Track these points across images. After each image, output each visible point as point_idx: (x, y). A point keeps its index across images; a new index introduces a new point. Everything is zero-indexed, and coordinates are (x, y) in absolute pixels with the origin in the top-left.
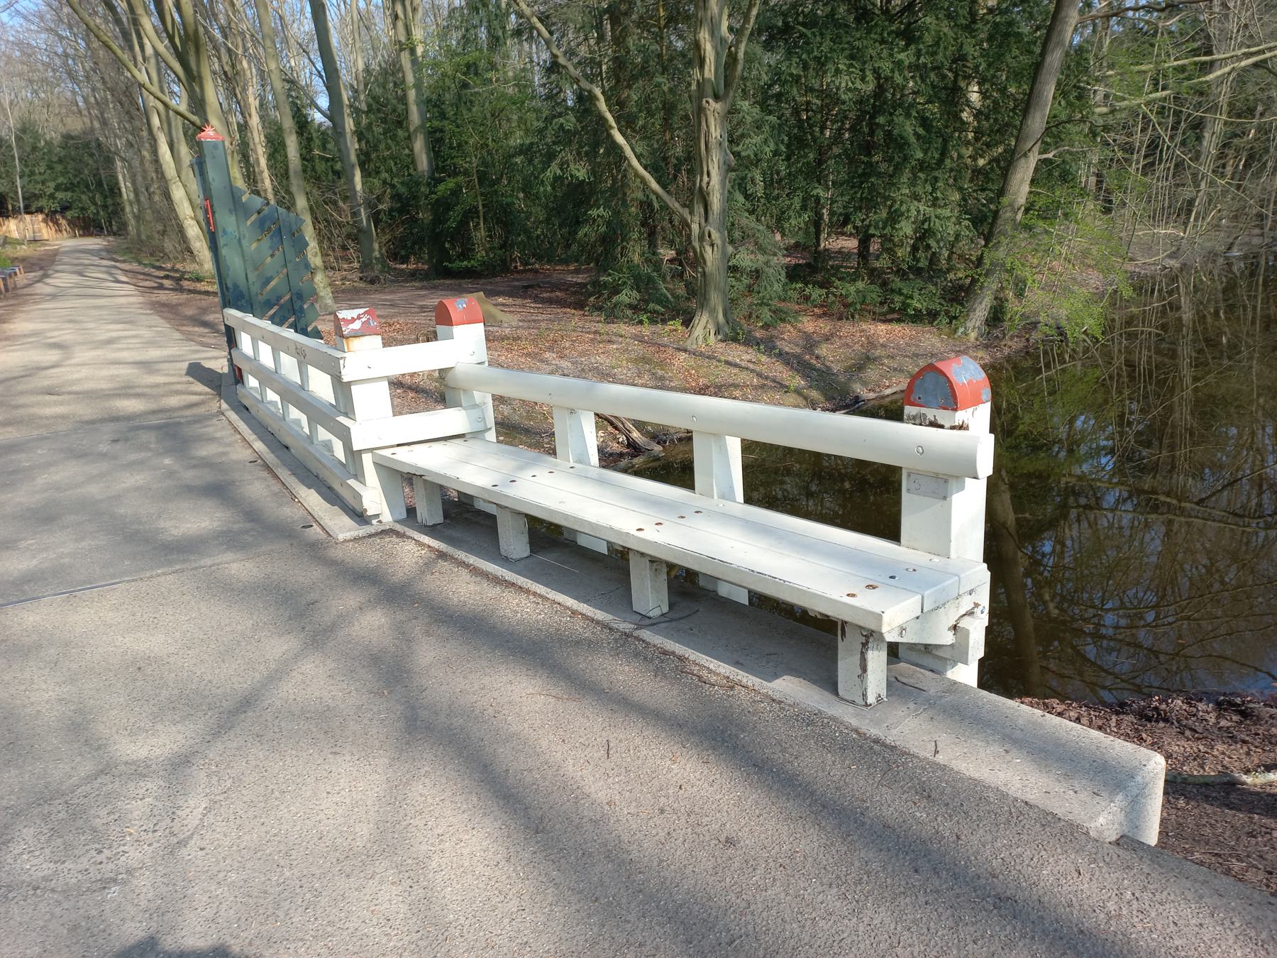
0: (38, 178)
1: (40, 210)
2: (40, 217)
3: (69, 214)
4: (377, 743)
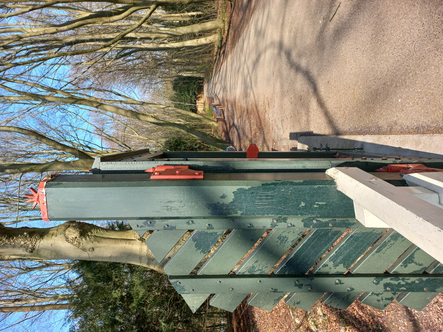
0: (186, 99)
1: (195, 101)
2: (197, 101)
3: (196, 93)
4: (103, 319)
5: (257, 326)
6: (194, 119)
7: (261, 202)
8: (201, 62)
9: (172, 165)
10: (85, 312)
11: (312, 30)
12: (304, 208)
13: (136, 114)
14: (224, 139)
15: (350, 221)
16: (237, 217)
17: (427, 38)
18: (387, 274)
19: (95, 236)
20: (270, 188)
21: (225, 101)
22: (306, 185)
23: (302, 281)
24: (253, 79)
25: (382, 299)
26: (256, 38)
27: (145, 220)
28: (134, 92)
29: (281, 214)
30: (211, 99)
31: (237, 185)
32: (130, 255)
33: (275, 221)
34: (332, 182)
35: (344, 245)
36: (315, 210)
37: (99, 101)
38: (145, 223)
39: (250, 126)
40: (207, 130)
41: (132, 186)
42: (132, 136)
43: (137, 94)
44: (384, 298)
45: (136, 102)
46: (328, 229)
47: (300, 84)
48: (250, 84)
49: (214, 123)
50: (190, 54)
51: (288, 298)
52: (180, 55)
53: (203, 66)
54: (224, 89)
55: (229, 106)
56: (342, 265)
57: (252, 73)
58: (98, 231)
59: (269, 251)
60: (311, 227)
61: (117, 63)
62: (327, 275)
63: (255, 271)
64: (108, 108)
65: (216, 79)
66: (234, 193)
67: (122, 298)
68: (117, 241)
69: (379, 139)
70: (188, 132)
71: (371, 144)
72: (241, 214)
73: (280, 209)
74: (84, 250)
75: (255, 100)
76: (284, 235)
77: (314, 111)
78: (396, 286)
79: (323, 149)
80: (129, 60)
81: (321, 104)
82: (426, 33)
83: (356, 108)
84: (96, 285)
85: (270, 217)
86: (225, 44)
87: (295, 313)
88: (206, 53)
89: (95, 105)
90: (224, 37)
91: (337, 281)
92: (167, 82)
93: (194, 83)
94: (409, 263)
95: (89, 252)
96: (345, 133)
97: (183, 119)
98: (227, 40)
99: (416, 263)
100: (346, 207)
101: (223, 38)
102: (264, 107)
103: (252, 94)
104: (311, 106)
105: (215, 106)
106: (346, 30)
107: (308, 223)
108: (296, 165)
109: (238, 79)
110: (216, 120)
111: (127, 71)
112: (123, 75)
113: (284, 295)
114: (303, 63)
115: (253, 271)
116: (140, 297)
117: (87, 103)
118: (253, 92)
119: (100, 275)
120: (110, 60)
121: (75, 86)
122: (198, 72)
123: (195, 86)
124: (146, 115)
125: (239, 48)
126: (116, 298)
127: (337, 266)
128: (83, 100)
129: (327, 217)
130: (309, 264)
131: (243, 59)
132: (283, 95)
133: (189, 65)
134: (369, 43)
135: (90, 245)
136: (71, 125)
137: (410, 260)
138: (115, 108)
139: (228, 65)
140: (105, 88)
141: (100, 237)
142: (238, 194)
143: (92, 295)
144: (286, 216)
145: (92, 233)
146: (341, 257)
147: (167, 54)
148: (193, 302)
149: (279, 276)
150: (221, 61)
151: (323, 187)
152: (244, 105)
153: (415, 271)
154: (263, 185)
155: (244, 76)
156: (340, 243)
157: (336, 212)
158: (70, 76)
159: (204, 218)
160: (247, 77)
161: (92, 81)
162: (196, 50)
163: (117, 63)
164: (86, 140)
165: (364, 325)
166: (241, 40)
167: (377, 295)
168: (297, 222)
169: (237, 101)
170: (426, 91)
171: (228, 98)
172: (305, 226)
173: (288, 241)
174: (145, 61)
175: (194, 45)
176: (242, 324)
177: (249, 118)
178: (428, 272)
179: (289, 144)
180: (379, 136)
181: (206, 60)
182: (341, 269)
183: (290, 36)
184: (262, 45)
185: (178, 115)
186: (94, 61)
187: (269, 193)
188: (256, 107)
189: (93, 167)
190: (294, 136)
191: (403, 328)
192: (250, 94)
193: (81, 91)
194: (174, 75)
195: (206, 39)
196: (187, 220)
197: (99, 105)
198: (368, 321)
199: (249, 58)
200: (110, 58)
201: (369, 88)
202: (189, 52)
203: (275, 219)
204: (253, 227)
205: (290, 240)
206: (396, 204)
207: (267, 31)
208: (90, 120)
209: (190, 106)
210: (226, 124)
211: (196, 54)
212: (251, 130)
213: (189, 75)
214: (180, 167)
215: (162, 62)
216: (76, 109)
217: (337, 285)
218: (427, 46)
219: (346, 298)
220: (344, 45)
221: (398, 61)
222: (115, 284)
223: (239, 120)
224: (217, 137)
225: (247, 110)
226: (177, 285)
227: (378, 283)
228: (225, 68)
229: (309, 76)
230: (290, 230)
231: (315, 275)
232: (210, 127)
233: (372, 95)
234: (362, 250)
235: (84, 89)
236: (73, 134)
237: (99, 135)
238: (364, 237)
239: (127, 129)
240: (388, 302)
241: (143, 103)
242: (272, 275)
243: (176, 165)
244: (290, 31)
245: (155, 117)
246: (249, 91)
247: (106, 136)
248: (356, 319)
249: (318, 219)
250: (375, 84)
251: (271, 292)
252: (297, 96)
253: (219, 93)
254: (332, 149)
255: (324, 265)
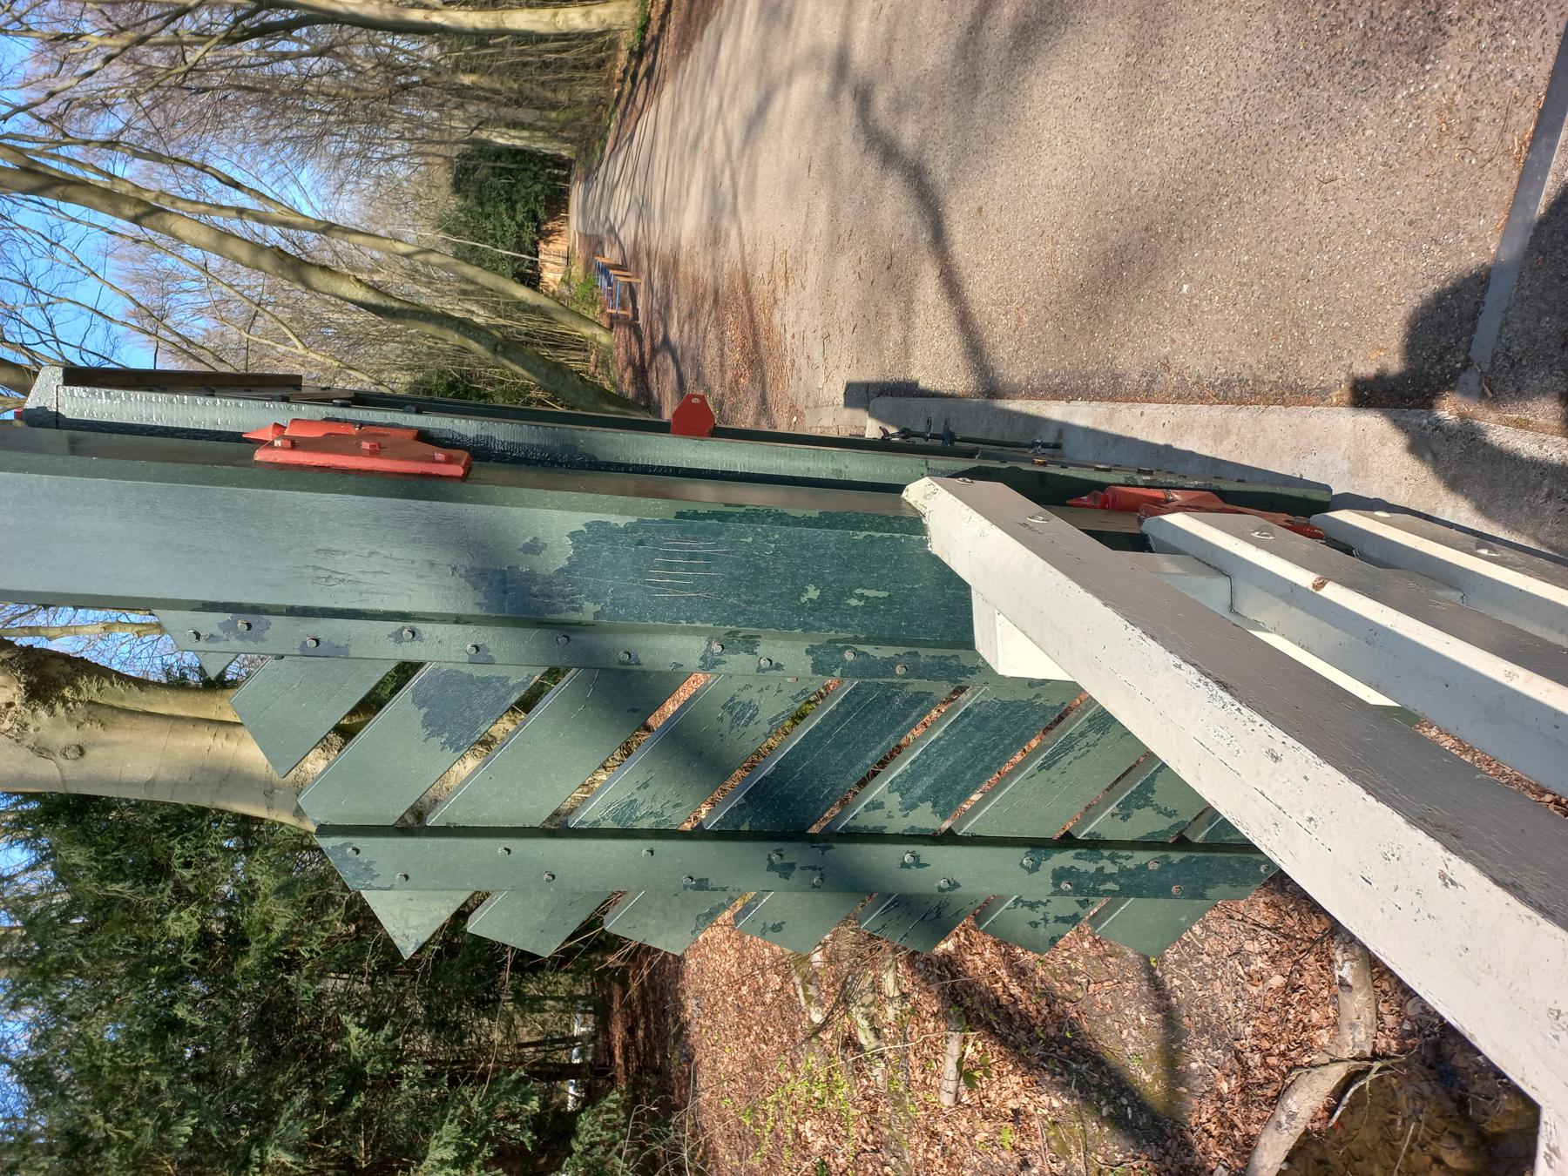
0: (499, 233)
1: (535, 244)
2: (542, 245)
3: (542, 215)
5: (688, 1036)
6: (524, 311)
7: (671, 577)
8: (562, 97)
9: (353, 422)
10: (54, 991)
11: (946, 17)
12: (816, 606)
13: (295, 266)
14: (629, 391)
15: (963, 662)
16: (579, 624)
17: (1283, 82)
18: (1067, 841)
19: (90, 702)
20: (703, 530)
21: (643, 256)
22: (829, 527)
23: (792, 852)
24: (741, 182)
25: (1046, 921)
26: (761, 29)
27: (228, 616)
28: (296, 181)
29: (737, 624)
30: (594, 244)
31: (586, 509)
32: (230, 778)
33: (717, 648)
34: (915, 524)
35: (939, 739)
36: (852, 617)
37: (147, 197)
38: (228, 628)
39: (722, 350)
40: (573, 355)
41: (176, 481)
42: (282, 348)
43: (309, 189)
44: (1051, 918)
45: (299, 220)
46: (891, 685)
47: (893, 207)
48: (730, 199)
49: (598, 331)
50: (525, 64)
51: (747, 908)
52: (486, 62)
53: (570, 114)
54: (642, 208)
55: (656, 273)
56: (927, 807)
57: (740, 158)
58: (107, 684)
59: (693, 748)
60: (837, 673)
61: (232, 58)
62: (878, 837)
63: (638, 819)
64: (182, 227)
65: (615, 169)
66: (572, 535)
67: (205, 940)
68: (179, 726)
69: (1111, 416)
70: (495, 351)
71: (1087, 431)
72: (596, 614)
73: (733, 606)
74: (42, 751)
75: (743, 262)
76: (744, 697)
77: (926, 310)
78: (1091, 877)
79: (934, 437)
80: (284, 56)
81: (952, 285)
82: (1281, 67)
83: (1054, 308)
84: (101, 892)
85: (697, 631)
86: (656, 40)
87: (812, 991)
88: (587, 68)
89: (129, 211)
90: (655, 14)
91: (907, 858)
92: (430, 160)
93: (536, 177)
94: (1138, 807)
95: (63, 762)
96: (1014, 392)
97: (484, 306)
98: (662, 28)
99: (1158, 810)
100: (947, 607)
101: (649, 19)
102: (771, 287)
103: (734, 233)
104: (920, 293)
105: (604, 270)
106: (1052, 28)
107: (827, 659)
108: (811, 464)
109: (691, 175)
110: (605, 322)
111: (278, 100)
112: (254, 110)
113: (732, 900)
114: (908, 134)
115: (629, 818)
116: (274, 936)
117: (96, 200)
118: (740, 229)
119: (120, 854)
120: (202, 44)
121: (50, 129)
122: (552, 134)
123: (538, 187)
124: (331, 271)
125: (702, 62)
126: (181, 940)
127: (913, 807)
128: (84, 184)
129: (891, 642)
130: (823, 801)
131: (713, 102)
132: (835, 245)
133: (518, 104)
134: (1116, 83)
135: (67, 735)
136: (25, 283)
137: (1142, 798)
138: (213, 234)
139: (662, 121)
140: (182, 154)
141: (112, 707)
142: (588, 541)
143: (87, 931)
144: (752, 630)
145: (78, 690)
146: (928, 781)
147: (435, 50)
148: (409, 921)
149: (720, 835)
150: (639, 103)
151: (882, 539)
152: (707, 275)
153: (1152, 834)
154: (680, 515)
155: (714, 168)
156: (926, 735)
157: (919, 626)
158: (27, 83)
159: (458, 620)
160: (722, 172)
161: (123, 116)
162: (549, 52)
163: (232, 58)
164: (89, 345)
165: (1020, 1028)
166: (710, 32)
167: (1032, 906)
168: (790, 655)
169: (683, 258)
170: (1262, 263)
171: (654, 244)
172: (819, 668)
173: (757, 719)
174: (348, 69)
175: (541, 28)
176: (640, 1033)
177: (719, 323)
178: (1189, 836)
179: (840, 421)
180: (1112, 405)
181: (585, 93)
182: (925, 818)
183: (873, 32)
184: (782, 57)
185: (464, 286)
186: (131, 35)
187: (701, 547)
188: (746, 283)
189: (31, 403)
190: (859, 395)
191: (1135, 1033)
192: (728, 236)
193: (76, 152)
194: (456, 136)
195: (587, 15)
196: (394, 626)
197: (148, 212)
198: (1034, 1013)
199: (732, 100)
200: (202, 36)
201: (1102, 239)
202: (521, 53)
203: (718, 640)
204: (638, 663)
205: (766, 714)
206: (1078, 588)
207: (799, 9)
208: (112, 270)
209: (515, 259)
210: (640, 340)
211: (545, 65)
212: (722, 365)
213: (518, 143)
214: (381, 431)
215: (415, 79)
216: (53, 220)
217: (906, 871)
218: (1282, 110)
219: (927, 915)
220: (1040, 81)
221: (1195, 153)
222: (179, 891)
223: (686, 327)
224: (607, 385)
225: (716, 292)
226: (347, 859)
227: (1034, 869)
228: (649, 130)
229: (921, 183)
230: (763, 682)
231: (839, 834)
232: (582, 345)
233: (1107, 266)
234: (995, 758)
235: (87, 143)
236: (38, 320)
237: (145, 332)
238: (1007, 718)
239: (260, 322)
240: (1061, 926)
241: (328, 228)
242: (698, 834)
243: (372, 424)
244: (875, 17)
245: (374, 288)
246: (725, 222)
247: (175, 339)
248: (1000, 1007)
249: (861, 648)
250: (1121, 228)
251: (685, 887)
252: (879, 252)
253: (623, 223)
254: (962, 440)
255: (872, 802)
